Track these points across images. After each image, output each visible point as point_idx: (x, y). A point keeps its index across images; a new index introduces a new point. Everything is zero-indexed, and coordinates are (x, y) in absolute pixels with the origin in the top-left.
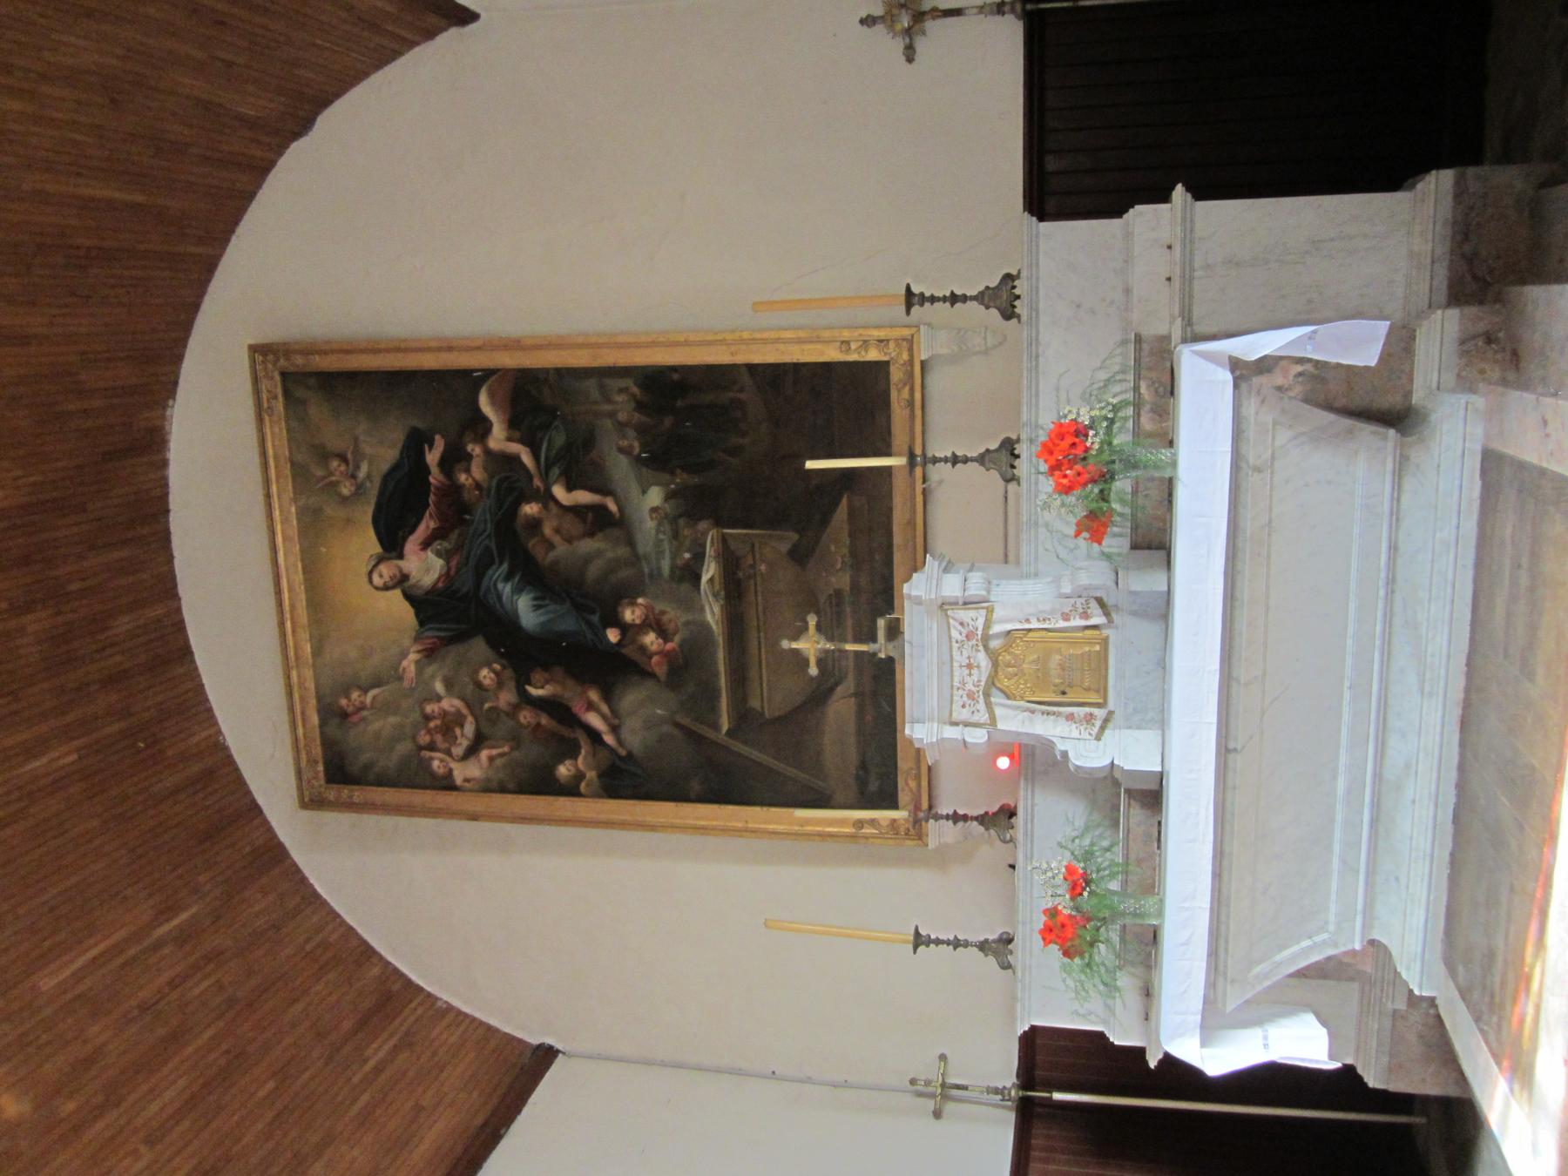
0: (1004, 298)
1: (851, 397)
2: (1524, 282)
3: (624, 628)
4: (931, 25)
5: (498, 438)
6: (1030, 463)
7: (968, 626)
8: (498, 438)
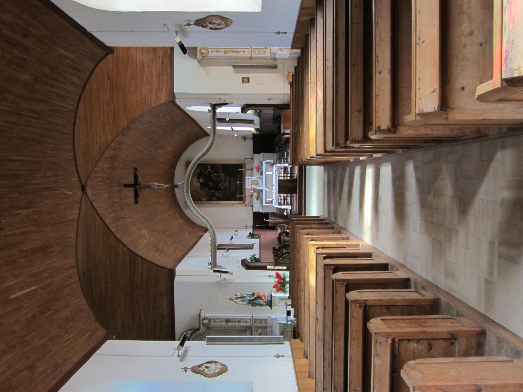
0: (252, 159)
1: (241, 166)
2: (392, 165)
3: (220, 186)
4: (251, 208)
5: (209, 169)
6: (255, 170)
7: (249, 182)
8: (209, 169)
